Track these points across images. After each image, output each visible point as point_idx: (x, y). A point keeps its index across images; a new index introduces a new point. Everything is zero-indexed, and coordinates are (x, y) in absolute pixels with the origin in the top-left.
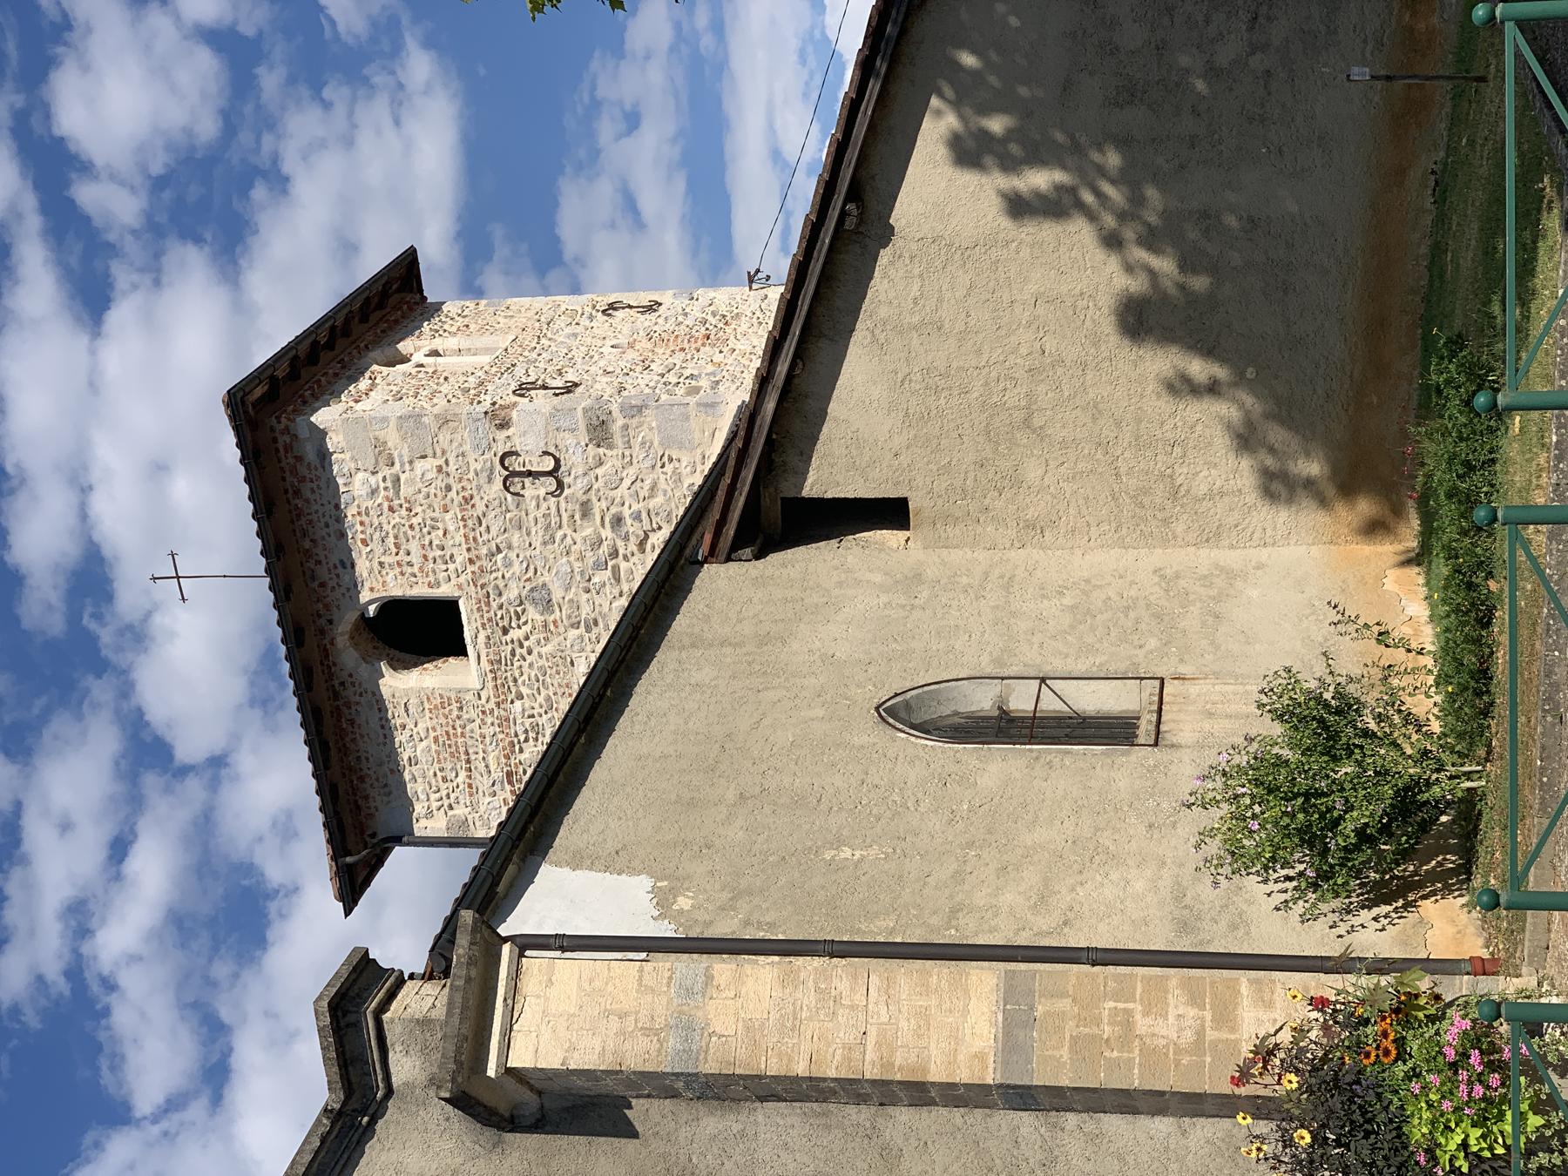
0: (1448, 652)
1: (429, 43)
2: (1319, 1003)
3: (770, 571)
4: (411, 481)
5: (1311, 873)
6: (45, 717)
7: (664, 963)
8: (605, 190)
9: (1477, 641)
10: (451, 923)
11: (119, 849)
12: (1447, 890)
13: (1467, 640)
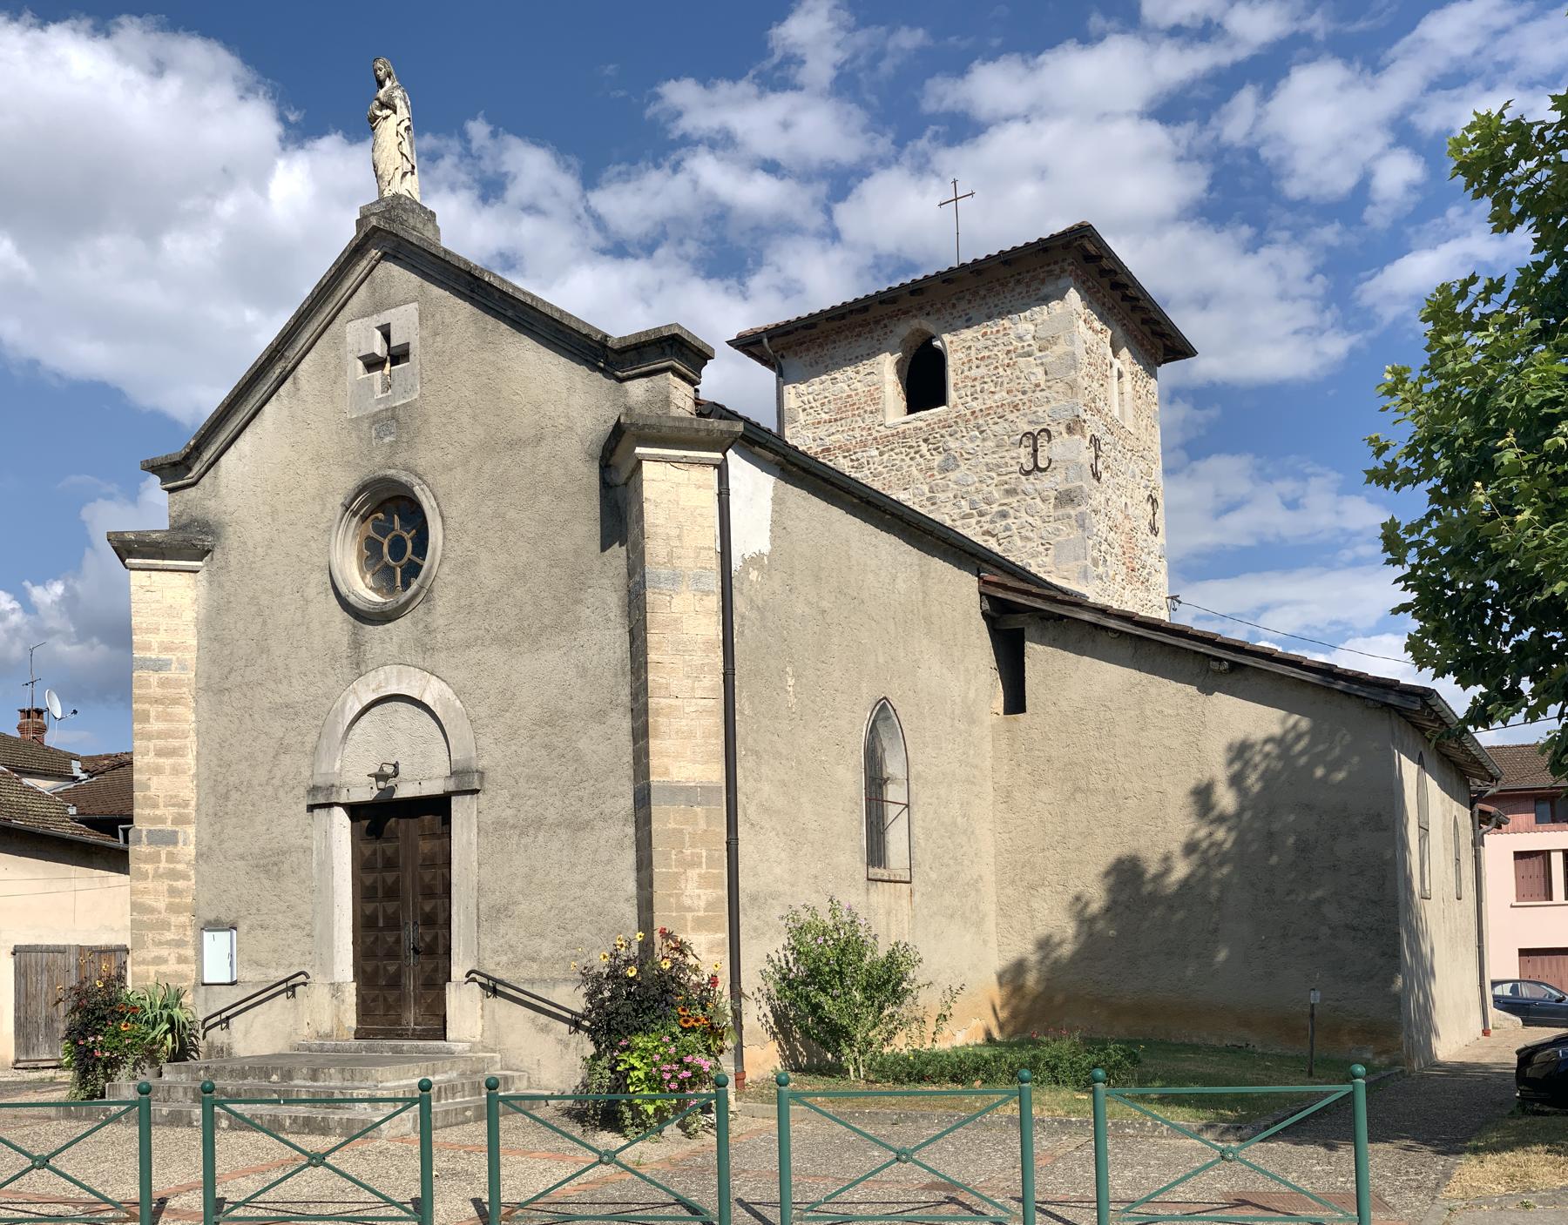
0: (935, 1057)
1: (1353, 352)
2: (714, 980)
3: (974, 622)
4: (1028, 365)
5: (791, 976)
6: (863, 105)
7: (715, 564)
8: (1243, 488)
11: (771, 167)
12: (785, 1058)
13: (943, 1068)
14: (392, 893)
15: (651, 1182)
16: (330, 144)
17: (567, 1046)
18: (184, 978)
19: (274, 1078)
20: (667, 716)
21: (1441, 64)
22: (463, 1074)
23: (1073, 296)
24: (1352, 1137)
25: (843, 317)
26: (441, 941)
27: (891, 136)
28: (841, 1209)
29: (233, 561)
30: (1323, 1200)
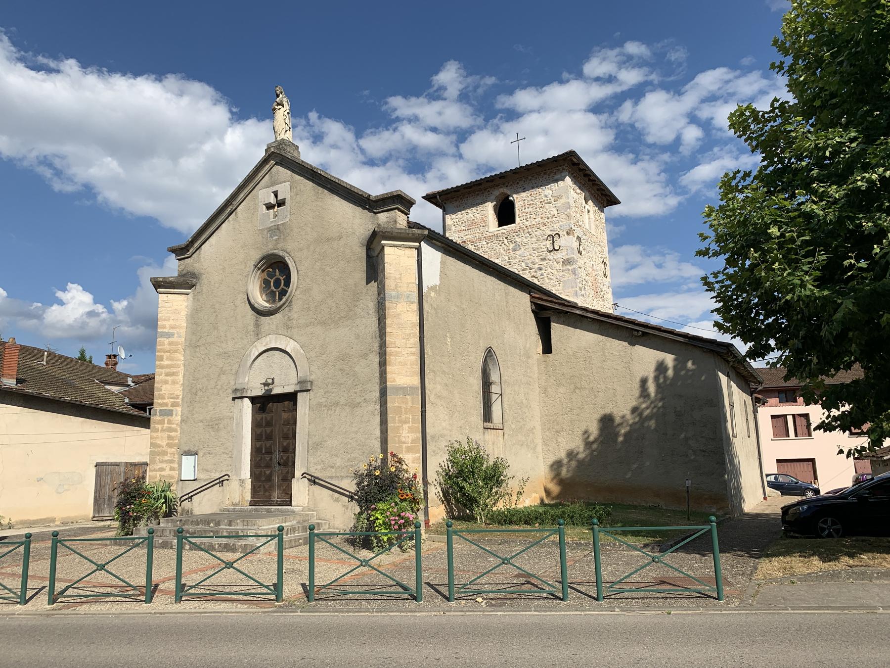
0: (517, 512)
1: (680, 204)
2: (415, 476)
6: (471, 105)
8: (638, 259)
9: (520, 520)
10: (424, 228)
11: (434, 130)
12: (448, 513)
14: (269, 437)
15: (384, 575)
16: (251, 123)
17: (347, 508)
18: (173, 477)
19: (212, 525)
20: (395, 356)
21: (704, 93)
22: (299, 522)
23: (568, 179)
24: (712, 551)
25: (471, 187)
26: (290, 459)
27: (483, 117)
28: (477, 587)
29: (204, 290)
30: (700, 581)
